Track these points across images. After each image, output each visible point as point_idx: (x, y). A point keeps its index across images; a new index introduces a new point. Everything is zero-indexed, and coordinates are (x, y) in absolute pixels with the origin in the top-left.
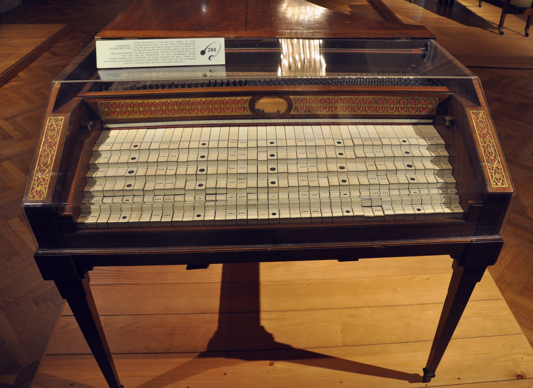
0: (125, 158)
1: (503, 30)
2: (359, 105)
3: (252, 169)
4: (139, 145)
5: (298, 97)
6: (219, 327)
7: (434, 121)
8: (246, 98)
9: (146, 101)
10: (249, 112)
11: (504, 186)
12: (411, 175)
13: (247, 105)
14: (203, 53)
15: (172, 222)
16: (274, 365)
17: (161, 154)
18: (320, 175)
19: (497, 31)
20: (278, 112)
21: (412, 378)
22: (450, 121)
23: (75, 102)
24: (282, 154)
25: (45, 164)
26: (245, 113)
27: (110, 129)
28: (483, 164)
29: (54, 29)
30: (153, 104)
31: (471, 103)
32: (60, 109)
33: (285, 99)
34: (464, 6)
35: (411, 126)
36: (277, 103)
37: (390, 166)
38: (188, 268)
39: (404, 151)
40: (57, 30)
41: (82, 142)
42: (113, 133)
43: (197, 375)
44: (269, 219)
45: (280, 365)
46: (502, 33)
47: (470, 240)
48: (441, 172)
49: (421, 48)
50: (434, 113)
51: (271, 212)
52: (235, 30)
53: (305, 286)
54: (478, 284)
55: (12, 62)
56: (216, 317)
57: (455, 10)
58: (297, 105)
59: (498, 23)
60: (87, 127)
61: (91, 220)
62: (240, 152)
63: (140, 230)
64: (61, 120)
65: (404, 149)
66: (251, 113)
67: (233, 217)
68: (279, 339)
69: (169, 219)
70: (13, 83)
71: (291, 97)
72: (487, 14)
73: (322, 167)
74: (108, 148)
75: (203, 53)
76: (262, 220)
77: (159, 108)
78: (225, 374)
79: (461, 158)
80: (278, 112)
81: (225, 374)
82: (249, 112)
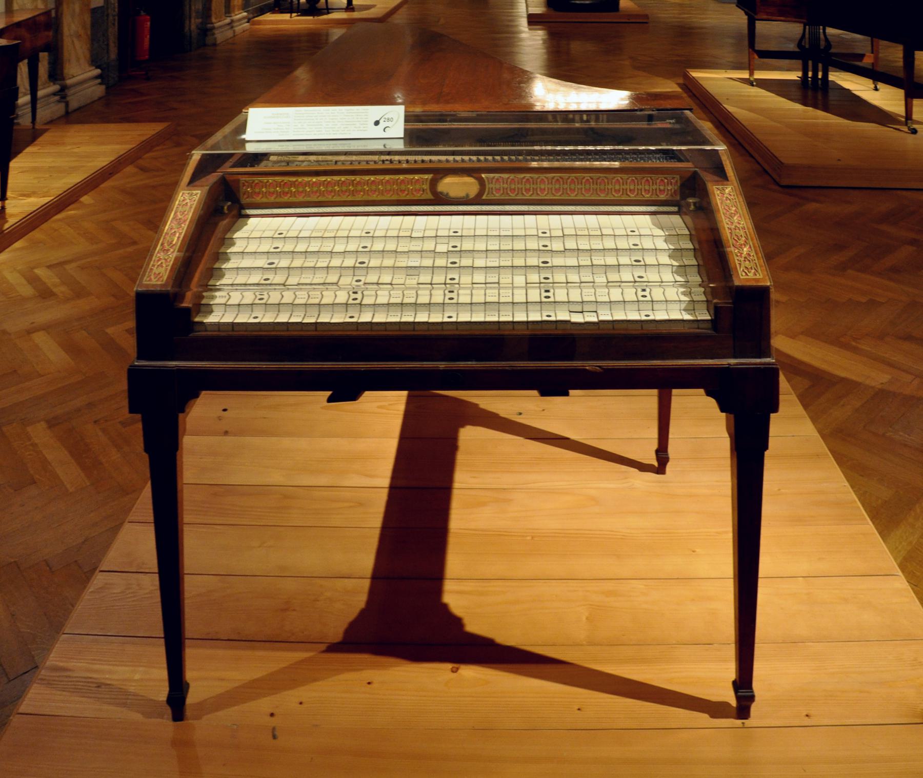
0: (266, 247)
1: (915, 126)
2: (573, 186)
3: (428, 262)
4: (285, 232)
5: (492, 175)
6: (369, 602)
7: (679, 209)
8: (426, 176)
9: (300, 180)
10: (429, 196)
11: (758, 277)
12: (639, 272)
13: (426, 186)
14: (377, 123)
15: (316, 323)
16: (460, 671)
17: (312, 244)
18: (515, 271)
19: (905, 129)
20: (467, 195)
21: (715, 709)
22: (695, 204)
23: (213, 178)
24: (467, 245)
25: (170, 243)
26: (424, 197)
27: (248, 216)
28: (729, 249)
29: (149, 130)
30: (308, 184)
31: (716, 178)
32: (197, 183)
33: (476, 178)
34: (848, 90)
35: (648, 217)
36: (465, 183)
37: (611, 260)
38: (330, 400)
39: (631, 244)
40: (153, 133)
41: (216, 225)
42: (252, 221)
43: (317, 683)
44: (443, 323)
45: (470, 673)
46: (914, 132)
47: (724, 361)
48: (682, 269)
49: (668, 121)
50: (678, 198)
51: (447, 315)
52: (424, 103)
53: (529, 538)
54: (766, 453)
55: (75, 179)
56: (366, 584)
57: (833, 96)
58: (491, 186)
59: (904, 114)
60: (223, 208)
61: (212, 319)
62: (414, 243)
63: (273, 333)
64: (196, 194)
65: (632, 241)
66: (432, 197)
67: (397, 319)
68: (473, 626)
69: (313, 320)
70: (70, 212)
71: (483, 176)
72: (889, 102)
73: (519, 262)
74: (246, 235)
75: (377, 123)
76: (433, 323)
77: (315, 189)
78: (369, 683)
79: (710, 253)
80: (467, 195)
81: (369, 683)
82: (429, 196)
